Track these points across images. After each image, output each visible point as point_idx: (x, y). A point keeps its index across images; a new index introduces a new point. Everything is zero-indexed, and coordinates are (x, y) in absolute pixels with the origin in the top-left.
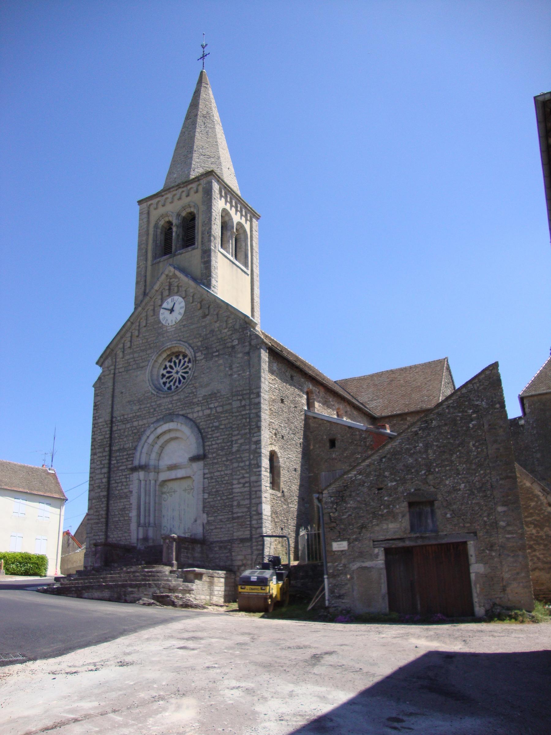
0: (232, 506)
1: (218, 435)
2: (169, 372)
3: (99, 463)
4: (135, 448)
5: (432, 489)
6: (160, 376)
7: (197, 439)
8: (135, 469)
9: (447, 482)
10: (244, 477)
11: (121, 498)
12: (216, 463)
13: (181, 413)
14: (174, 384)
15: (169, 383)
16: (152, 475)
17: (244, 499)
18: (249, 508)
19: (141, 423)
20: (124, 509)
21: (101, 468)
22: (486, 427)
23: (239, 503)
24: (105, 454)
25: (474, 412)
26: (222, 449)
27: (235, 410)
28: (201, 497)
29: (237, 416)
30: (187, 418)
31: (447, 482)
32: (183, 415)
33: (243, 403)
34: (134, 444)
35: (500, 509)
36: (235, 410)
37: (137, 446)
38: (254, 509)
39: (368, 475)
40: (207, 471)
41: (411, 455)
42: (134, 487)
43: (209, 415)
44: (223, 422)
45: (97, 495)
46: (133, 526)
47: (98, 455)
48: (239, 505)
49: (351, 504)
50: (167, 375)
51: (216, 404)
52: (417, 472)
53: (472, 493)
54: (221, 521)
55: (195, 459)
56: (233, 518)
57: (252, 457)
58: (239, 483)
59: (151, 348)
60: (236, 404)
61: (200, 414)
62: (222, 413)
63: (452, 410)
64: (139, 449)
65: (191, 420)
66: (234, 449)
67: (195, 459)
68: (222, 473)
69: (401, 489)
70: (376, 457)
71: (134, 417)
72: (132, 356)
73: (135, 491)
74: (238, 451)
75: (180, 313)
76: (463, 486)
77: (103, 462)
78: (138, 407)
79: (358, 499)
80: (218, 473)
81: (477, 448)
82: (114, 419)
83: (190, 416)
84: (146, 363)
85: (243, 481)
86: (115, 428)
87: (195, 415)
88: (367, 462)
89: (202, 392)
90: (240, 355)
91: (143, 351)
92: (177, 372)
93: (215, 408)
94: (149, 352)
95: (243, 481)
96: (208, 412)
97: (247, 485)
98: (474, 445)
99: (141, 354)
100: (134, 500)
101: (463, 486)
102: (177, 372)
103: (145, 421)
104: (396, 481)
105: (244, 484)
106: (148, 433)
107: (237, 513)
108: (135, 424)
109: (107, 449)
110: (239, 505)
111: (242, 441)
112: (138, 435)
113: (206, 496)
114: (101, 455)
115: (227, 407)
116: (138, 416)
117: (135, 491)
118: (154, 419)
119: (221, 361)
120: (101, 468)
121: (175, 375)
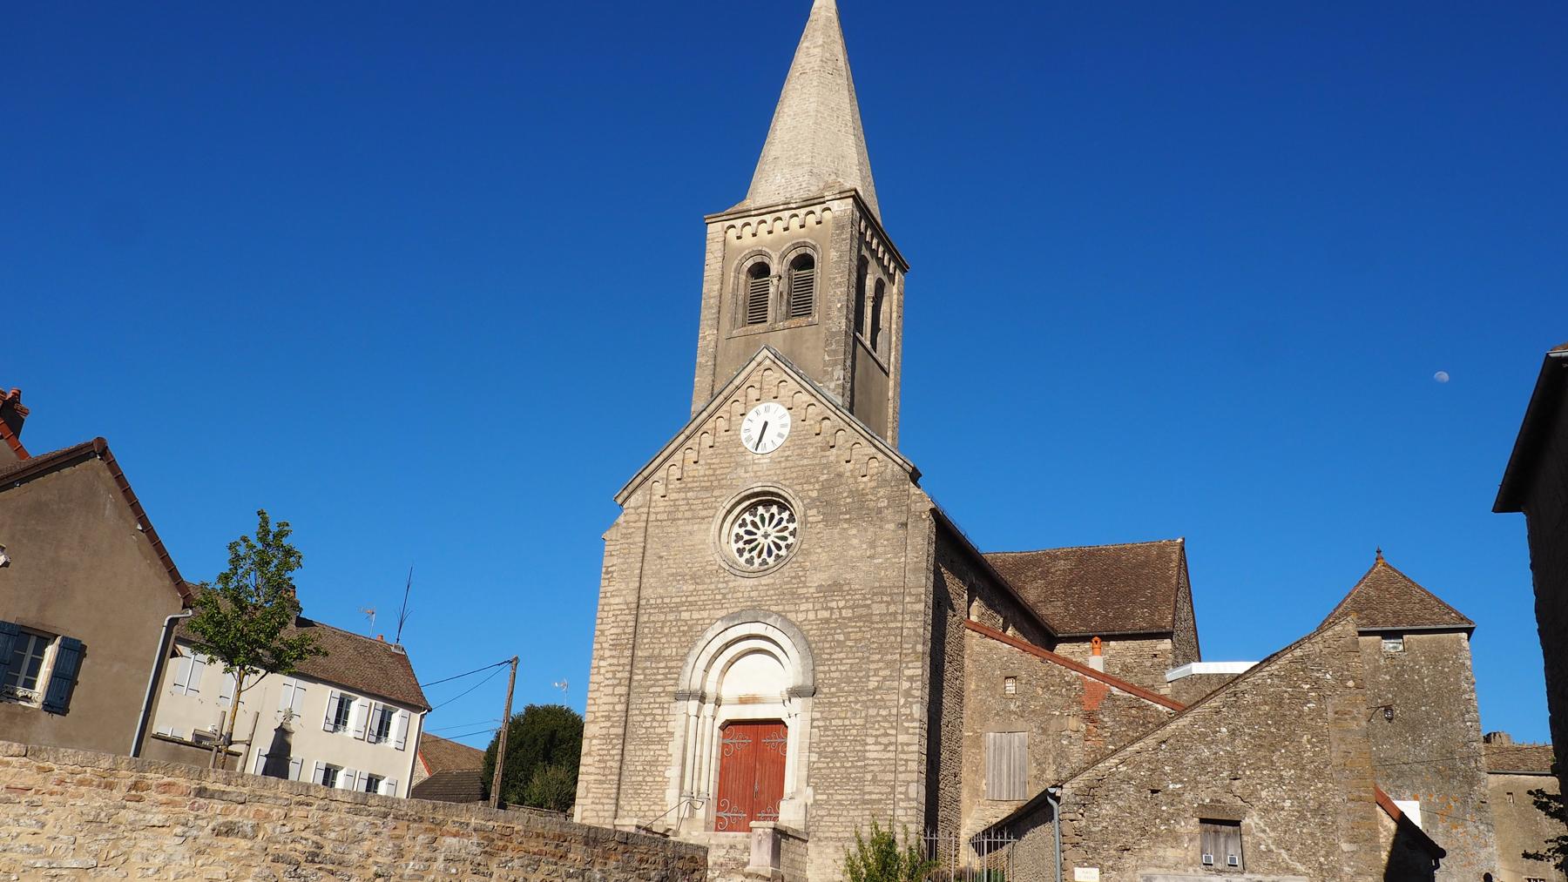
0: (862, 780)
1: (842, 655)
2: (748, 533)
3: (609, 675)
4: (683, 658)
5: (1240, 803)
6: (733, 538)
7: (802, 658)
8: (681, 696)
9: (1264, 794)
10: (886, 735)
11: (650, 742)
12: (836, 704)
13: (774, 608)
14: (751, 551)
15: (751, 551)
16: (709, 708)
17: (883, 771)
18: (893, 787)
19: (696, 615)
20: (653, 763)
21: (614, 686)
22: (1331, 715)
23: (875, 777)
24: (622, 661)
25: (1312, 689)
26: (849, 682)
27: (877, 618)
28: (805, 760)
29: (879, 630)
30: (785, 618)
31: (1264, 794)
32: (778, 613)
33: (892, 608)
34: (681, 652)
35: (1345, 847)
36: (877, 618)
37: (686, 655)
38: (903, 789)
39: (1138, 766)
40: (818, 715)
41: (1208, 745)
42: (677, 726)
43: (827, 621)
44: (853, 636)
45: (604, 731)
46: (672, 794)
47: (611, 661)
48: (874, 780)
49: (1107, 809)
50: (747, 537)
51: (841, 604)
52: (1216, 773)
53: (1302, 817)
54: (840, 803)
55: (795, 693)
56: (865, 802)
57: (902, 701)
58: (877, 743)
59: (721, 487)
60: (878, 609)
61: (811, 616)
62: (850, 619)
63: (1276, 681)
64: (691, 660)
65: (793, 624)
66: (872, 685)
67: (795, 693)
68: (847, 722)
69: (1188, 796)
70: (1150, 741)
71: (682, 604)
72: (682, 495)
73: (679, 733)
74: (878, 688)
75: (780, 435)
76: (1288, 803)
77: (619, 675)
78: (692, 588)
79: (1120, 804)
80: (839, 722)
81: (1314, 746)
82: (643, 602)
83: (792, 616)
84: (712, 512)
85: (884, 740)
86: (644, 618)
87: (801, 617)
88: (1136, 747)
89: (817, 579)
90: (892, 526)
91: (706, 489)
92: (766, 536)
93: (840, 609)
94: (716, 493)
95: (884, 740)
96: (826, 614)
97: (892, 748)
98: (1309, 741)
99: (703, 494)
100: (675, 748)
101: (1288, 803)
102: (766, 536)
103: (705, 614)
104: (1181, 782)
105: (886, 746)
106: (709, 635)
107: (870, 793)
108: (685, 615)
109: (628, 653)
110: (874, 780)
111: (887, 672)
112: (690, 636)
113: (814, 757)
114: (615, 661)
115: (864, 611)
116: (691, 603)
117: (679, 733)
118: (723, 613)
119: (854, 531)
120: (614, 686)
121: (761, 540)
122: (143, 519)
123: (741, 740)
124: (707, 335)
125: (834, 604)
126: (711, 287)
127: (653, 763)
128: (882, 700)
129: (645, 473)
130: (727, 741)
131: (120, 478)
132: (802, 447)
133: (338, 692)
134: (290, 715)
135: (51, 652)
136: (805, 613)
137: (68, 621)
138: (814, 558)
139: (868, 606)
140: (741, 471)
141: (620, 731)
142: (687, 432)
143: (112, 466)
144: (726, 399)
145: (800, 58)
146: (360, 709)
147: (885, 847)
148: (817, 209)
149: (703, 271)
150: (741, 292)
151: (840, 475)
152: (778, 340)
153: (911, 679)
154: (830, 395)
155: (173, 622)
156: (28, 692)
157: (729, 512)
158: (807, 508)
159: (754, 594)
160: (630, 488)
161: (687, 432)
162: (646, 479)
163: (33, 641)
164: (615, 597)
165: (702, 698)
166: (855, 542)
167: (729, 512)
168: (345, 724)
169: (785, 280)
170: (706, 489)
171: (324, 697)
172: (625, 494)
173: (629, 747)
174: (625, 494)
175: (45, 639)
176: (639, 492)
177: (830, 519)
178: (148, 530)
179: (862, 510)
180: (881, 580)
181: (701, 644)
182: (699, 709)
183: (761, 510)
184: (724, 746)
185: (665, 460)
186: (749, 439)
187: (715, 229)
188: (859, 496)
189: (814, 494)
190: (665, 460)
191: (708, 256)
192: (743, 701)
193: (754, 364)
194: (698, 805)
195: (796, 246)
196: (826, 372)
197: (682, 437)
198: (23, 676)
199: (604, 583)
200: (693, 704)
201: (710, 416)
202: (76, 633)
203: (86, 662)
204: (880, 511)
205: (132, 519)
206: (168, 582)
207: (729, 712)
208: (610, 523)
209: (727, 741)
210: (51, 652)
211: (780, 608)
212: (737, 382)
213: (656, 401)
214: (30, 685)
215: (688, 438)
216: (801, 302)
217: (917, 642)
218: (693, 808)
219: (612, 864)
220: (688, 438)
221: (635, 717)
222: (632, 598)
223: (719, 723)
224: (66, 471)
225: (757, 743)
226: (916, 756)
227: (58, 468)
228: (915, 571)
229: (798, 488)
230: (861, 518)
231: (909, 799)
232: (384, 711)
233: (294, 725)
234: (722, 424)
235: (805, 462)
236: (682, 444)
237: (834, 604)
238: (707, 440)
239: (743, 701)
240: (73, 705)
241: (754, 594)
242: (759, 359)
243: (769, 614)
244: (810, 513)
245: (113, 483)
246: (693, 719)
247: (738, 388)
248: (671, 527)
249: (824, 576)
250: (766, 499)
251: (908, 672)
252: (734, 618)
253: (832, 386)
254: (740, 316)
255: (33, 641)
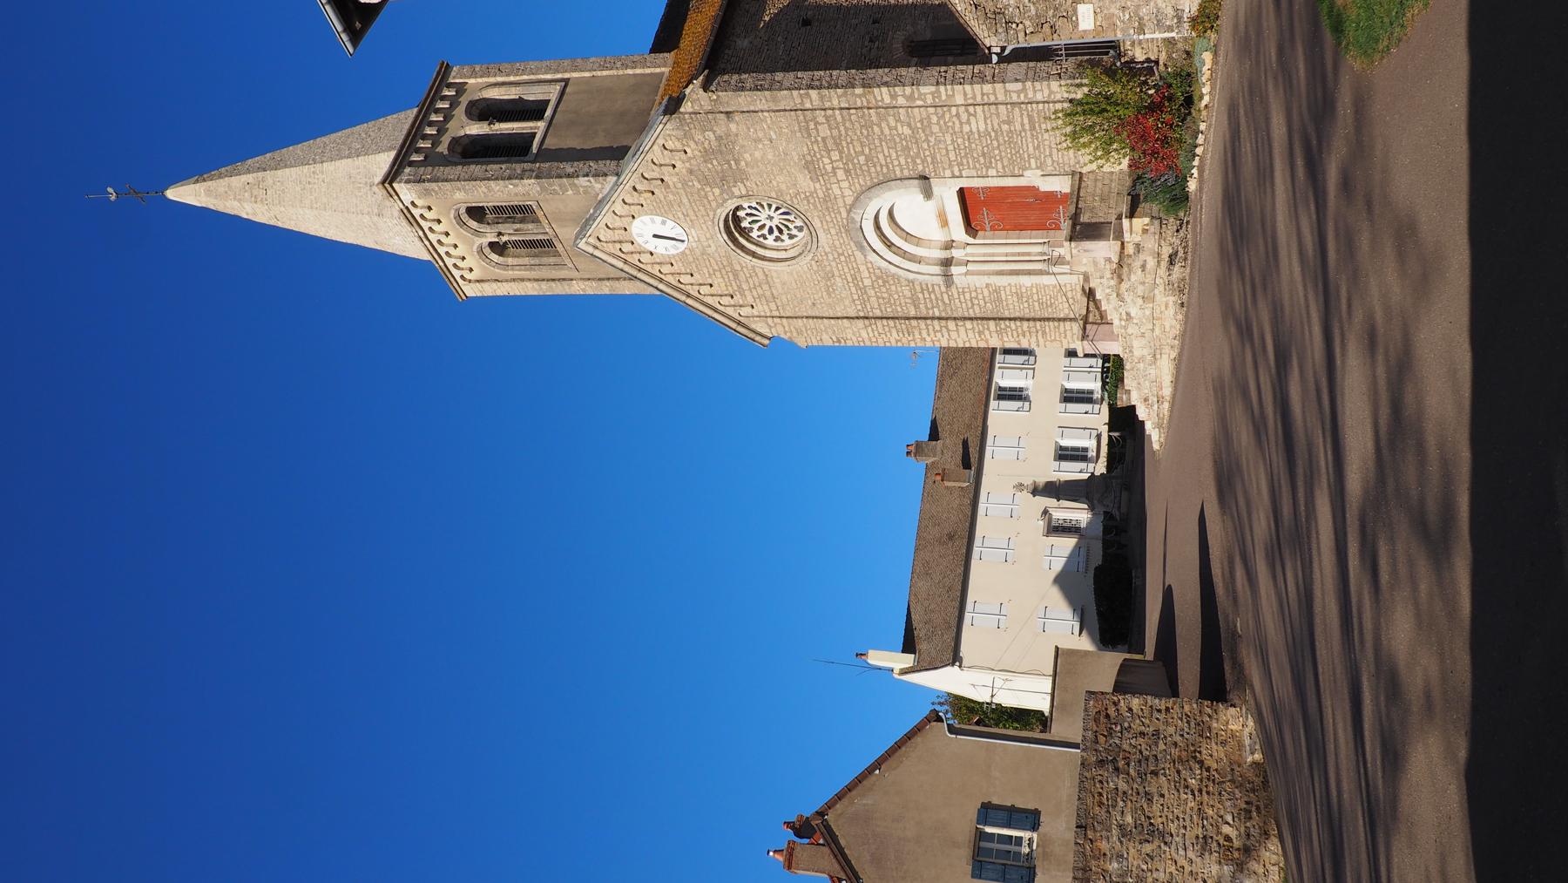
8: (948, 277)
10: (958, 115)
13: (844, 215)
16: (957, 253)
20: (1019, 296)
26: (907, 148)
27: (835, 132)
29: (846, 129)
30: (853, 205)
32: (849, 212)
36: (835, 132)
43: (847, 171)
44: (858, 149)
48: (1009, 122)
51: (826, 161)
58: (968, 122)
60: (824, 131)
62: (841, 152)
64: (911, 276)
65: (857, 199)
66: (907, 131)
74: (909, 125)
75: (664, 223)
83: (849, 200)
85: (964, 117)
87: (847, 192)
89: (805, 183)
90: (733, 127)
91: (736, 276)
92: (771, 218)
94: (738, 267)
95: (964, 117)
96: (840, 174)
99: (742, 277)
103: (862, 268)
108: (867, 282)
109: (914, 323)
111: (891, 119)
115: (830, 143)
117: (986, 280)
118: (858, 254)
122: (869, 771)
123: (985, 216)
124: (577, 288)
125: (829, 168)
126: (530, 289)
127: (1019, 296)
128: (921, 121)
129: (734, 325)
130: (988, 227)
131: (840, 797)
132: (670, 204)
133: (993, 404)
134: (1020, 487)
135: (989, 830)
136: (844, 189)
137: (963, 821)
138: (783, 187)
139: (824, 139)
140: (709, 251)
141: (992, 323)
142: (683, 298)
143: (830, 805)
144: (640, 270)
145: (261, 218)
146: (1005, 378)
147: (1078, 108)
148: (416, 212)
149: (515, 297)
150: (526, 260)
151: (691, 172)
152: (566, 233)
153: (894, 97)
154: (608, 188)
155: (951, 729)
156: (1025, 843)
157: (754, 254)
158: (733, 196)
159: (833, 231)
160: (751, 335)
161: (683, 298)
162: (739, 323)
163: (984, 844)
164: (858, 335)
165: (947, 263)
166: (758, 154)
167: (754, 254)
168: (1021, 389)
169: (501, 228)
170: (736, 276)
171: (1000, 416)
172: (758, 338)
173: (1007, 314)
174: (758, 338)
175: (981, 836)
176: (753, 326)
177: (741, 177)
178: (878, 764)
179: (724, 149)
180: (793, 132)
181: (893, 269)
182: (960, 264)
183: (745, 224)
184: (993, 229)
185: (716, 310)
186: (675, 247)
187: (471, 291)
188: (707, 154)
189: (717, 191)
190: (716, 310)
191: (499, 293)
192: (944, 223)
193: (597, 253)
194: (1056, 254)
195: (462, 224)
196: (586, 192)
197: (689, 301)
198: (1013, 848)
199: (849, 343)
200: (954, 270)
201: (661, 280)
202: (973, 814)
203: (995, 801)
204: (719, 138)
205: (872, 779)
206: (918, 739)
207: (958, 231)
208: (789, 345)
209: (988, 227)
210: (989, 830)
211: (843, 211)
212: (620, 264)
213: (656, 324)
214: (1019, 840)
215: (689, 296)
216: (520, 213)
217: (853, 94)
218: (1060, 261)
219: (1104, 846)
220: (689, 296)
221: (977, 312)
222: (860, 323)
223: (971, 240)
224: (843, 842)
225: (985, 203)
226: (977, 87)
227: (841, 850)
228: (775, 100)
229: (714, 204)
230: (731, 151)
231: (1024, 89)
232: (1000, 398)
233: (1028, 481)
234: (666, 269)
235: (685, 201)
236: (696, 299)
237: (829, 168)
238: (686, 279)
239: (944, 223)
240: (1031, 806)
241: (833, 231)
242: (590, 250)
243: (851, 220)
244: (737, 193)
245: (845, 801)
246: (971, 267)
247: (626, 262)
248: (785, 296)
249: (800, 177)
250: (734, 226)
251: (887, 100)
252: (863, 245)
253: (598, 186)
254: (552, 260)
255: (984, 844)
